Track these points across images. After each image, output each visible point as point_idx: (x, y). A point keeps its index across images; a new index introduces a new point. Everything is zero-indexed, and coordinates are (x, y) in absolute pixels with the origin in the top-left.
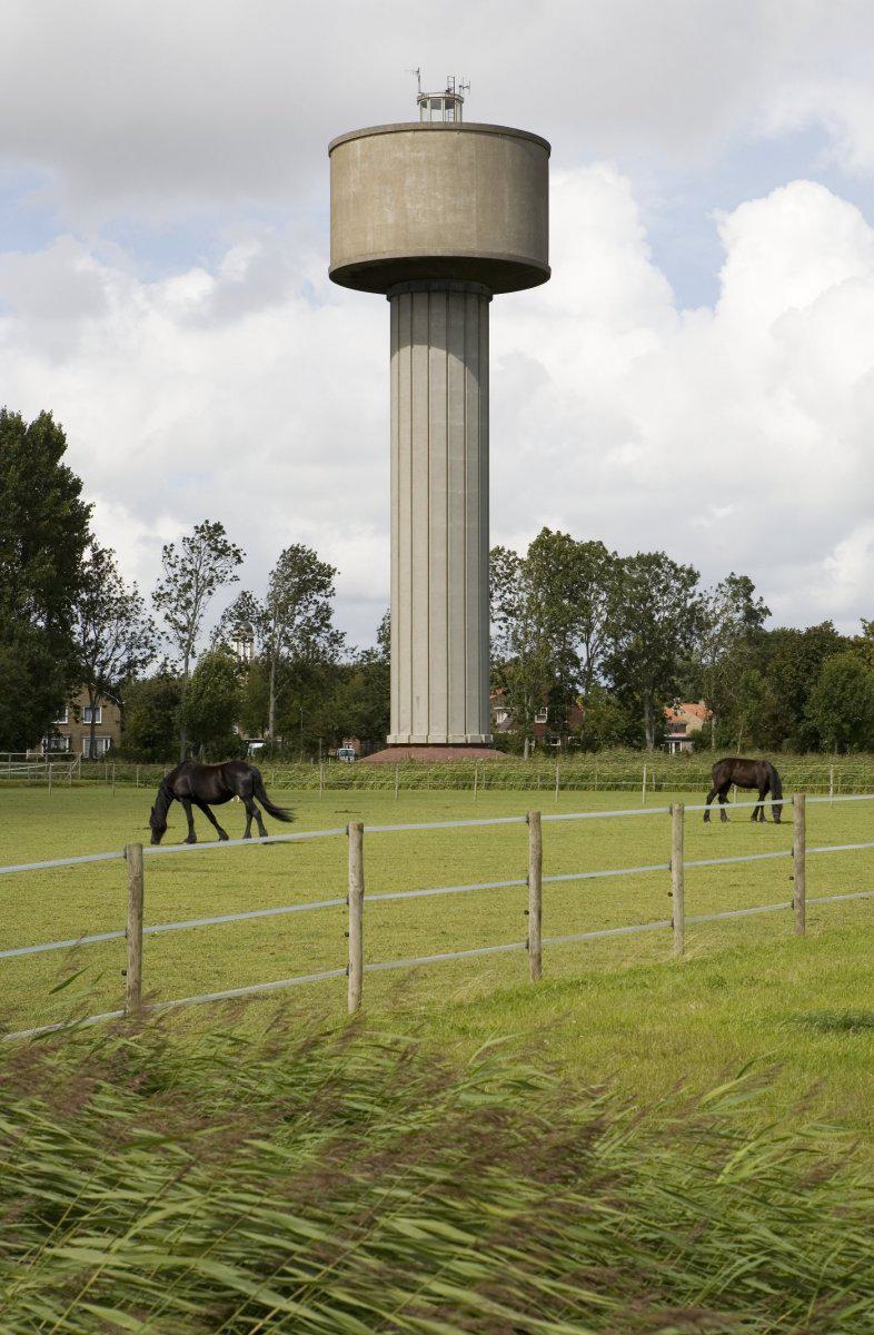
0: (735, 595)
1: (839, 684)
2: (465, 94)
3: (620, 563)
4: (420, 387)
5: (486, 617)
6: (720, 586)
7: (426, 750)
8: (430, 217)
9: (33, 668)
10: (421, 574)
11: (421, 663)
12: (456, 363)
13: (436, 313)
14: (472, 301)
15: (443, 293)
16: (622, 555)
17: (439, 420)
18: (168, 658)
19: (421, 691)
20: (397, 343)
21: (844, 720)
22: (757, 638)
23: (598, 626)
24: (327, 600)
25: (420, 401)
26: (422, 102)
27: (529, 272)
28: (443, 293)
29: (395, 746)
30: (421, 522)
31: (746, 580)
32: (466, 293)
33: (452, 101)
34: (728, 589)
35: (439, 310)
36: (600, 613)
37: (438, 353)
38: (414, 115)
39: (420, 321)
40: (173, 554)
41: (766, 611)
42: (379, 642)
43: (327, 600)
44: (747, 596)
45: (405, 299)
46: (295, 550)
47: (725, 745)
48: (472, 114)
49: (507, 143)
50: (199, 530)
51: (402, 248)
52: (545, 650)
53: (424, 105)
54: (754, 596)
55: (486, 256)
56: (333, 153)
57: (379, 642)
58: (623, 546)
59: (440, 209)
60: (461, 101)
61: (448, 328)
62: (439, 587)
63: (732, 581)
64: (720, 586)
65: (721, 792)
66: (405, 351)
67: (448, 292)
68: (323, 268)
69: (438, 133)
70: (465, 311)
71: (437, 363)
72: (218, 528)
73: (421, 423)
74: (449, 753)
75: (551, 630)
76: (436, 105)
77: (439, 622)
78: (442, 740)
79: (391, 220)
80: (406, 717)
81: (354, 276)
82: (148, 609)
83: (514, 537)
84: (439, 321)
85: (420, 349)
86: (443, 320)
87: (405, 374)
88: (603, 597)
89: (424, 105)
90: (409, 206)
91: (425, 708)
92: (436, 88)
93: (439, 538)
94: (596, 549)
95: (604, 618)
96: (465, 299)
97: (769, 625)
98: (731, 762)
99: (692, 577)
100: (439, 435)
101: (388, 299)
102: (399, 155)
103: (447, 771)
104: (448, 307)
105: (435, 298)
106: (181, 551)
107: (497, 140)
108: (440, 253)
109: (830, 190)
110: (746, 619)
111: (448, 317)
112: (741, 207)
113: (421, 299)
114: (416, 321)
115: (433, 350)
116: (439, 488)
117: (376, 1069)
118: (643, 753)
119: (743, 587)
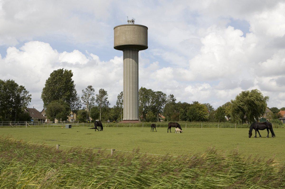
0: (171, 97)
1: (192, 111)
2: (134, 20)
3: (154, 92)
4: (128, 64)
5: (138, 101)
6: (169, 96)
7: (129, 121)
8: (130, 39)
9: (66, 108)
10: (128, 93)
11: (128, 108)
12: (134, 61)
13: (131, 53)
14: (136, 52)
15: (131, 50)
16: (154, 91)
17: (131, 70)
18: (84, 106)
19: (128, 112)
20: (124, 58)
21: (193, 116)
22: (174, 104)
23: (151, 102)
24: (107, 97)
25: (128, 67)
26: (128, 21)
27: (144, 47)
28: (131, 50)
29: (124, 120)
30: (128, 86)
31: (173, 95)
32: (135, 50)
33: (133, 21)
34: (170, 97)
35: (131, 53)
36: (151, 100)
37: (131, 59)
38: (127, 23)
39: (128, 54)
40: (84, 91)
41: (176, 100)
42: (116, 104)
43: (107, 97)
44: (173, 98)
45: (126, 51)
46: (101, 90)
47: (170, 120)
48: (136, 23)
49: (142, 28)
50: (88, 87)
51: (126, 43)
52: (142, 105)
53: (129, 22)
54: (174, 98)
55: (139, 45)
56: (115, 29)
57: (116, 104)
58: (155, 90)
59: (132, 37)
60: (134, 21)
61: (132, 56)
62: (131, 96)
63: (171, 95)
64: (169, 96)
65: (170, 127)
66: (126, 59)
67: (132, 50)
68: (113, 46)
69: (131, 26)
70: (135, 53)
71: (131, 61)
72: (91, 86)
73: (128, 70)
74: (133, 122)
75: (143, 103)
76: (130, 22)
77: (131, 101)
78: (126, 120)
79: (124, 39)
80: (126, 116)
81: (118, 48)
82: (80, 99)
83: (140, 88)
84: (131, 54)
85: (128, 59)
86: (132, 54)
87: (126, 63)
88: (151, 97)
89: (129, 22)
90: (127, 37)
91: (129, 113)
92: (130, 19)
93: (131, 88)
94: (150, 90)
95: (151, 101)
96: (130, 51)
97: (176, 102)
98: (171, 123)
99: (165, 95)
100: (131, 72)
101: (123, 51)
102: (125, 29)
103: (129, 124)
104: (132, 52)
105: (128, 51)
106: (85, 90)
107: (140, 27)
108: (132, 44)
109: (50, 45)
110: (173, 101)
111: (132, 54)
112: (243, 33)
113: (128, 51)
114: (127, 55)
115: (130, 59)
116: (131, 80)
117: (199, 178)
118: (186, 121)
119: (172, 96)
